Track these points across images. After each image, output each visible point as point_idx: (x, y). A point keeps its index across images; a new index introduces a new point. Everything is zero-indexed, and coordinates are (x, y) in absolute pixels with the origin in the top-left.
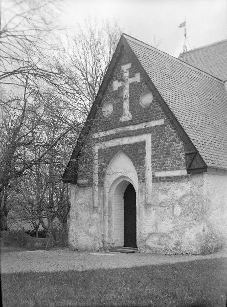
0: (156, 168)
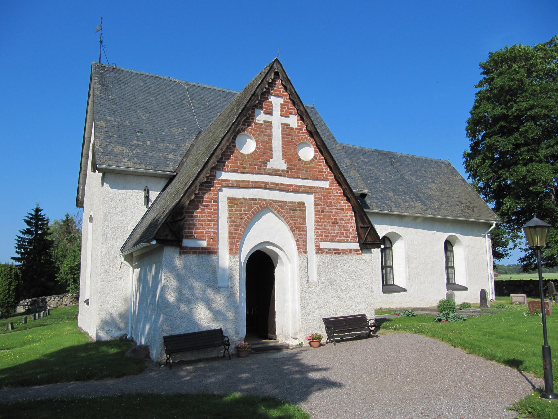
0: (322, 236)
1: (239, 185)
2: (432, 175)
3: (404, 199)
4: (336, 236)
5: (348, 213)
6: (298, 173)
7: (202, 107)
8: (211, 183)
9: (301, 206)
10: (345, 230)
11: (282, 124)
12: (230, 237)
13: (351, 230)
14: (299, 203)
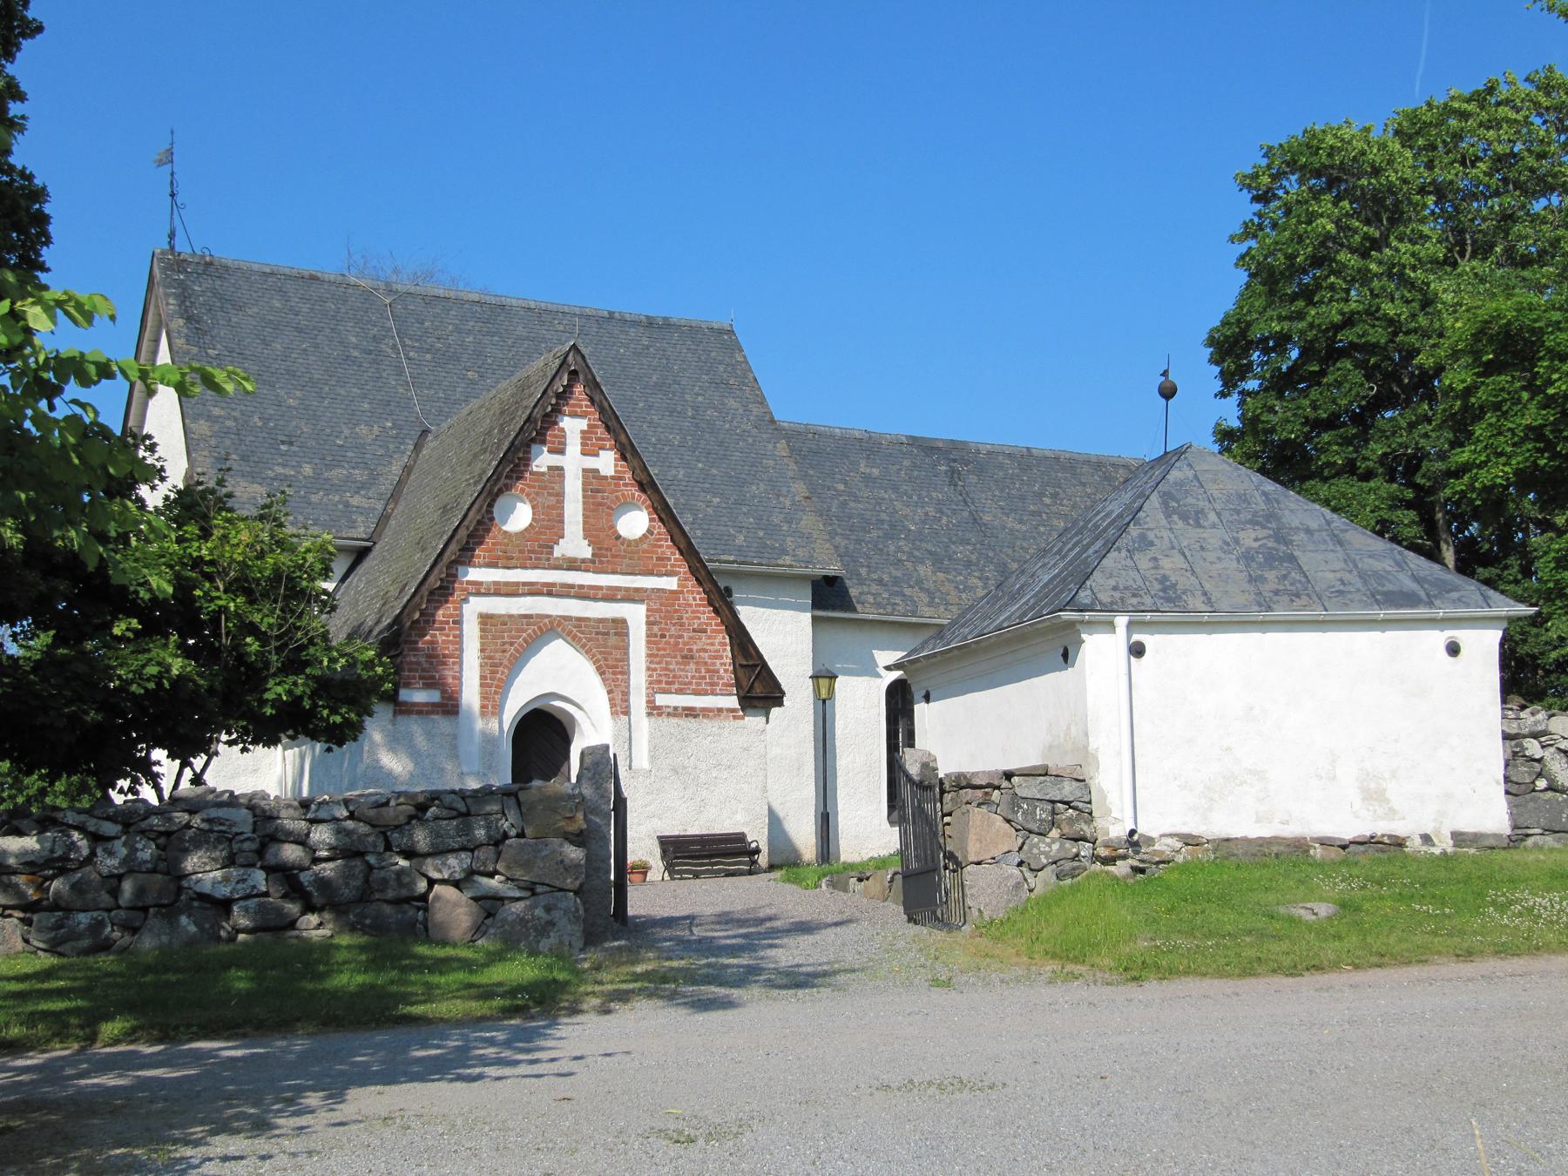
1: (499, 590)
2: (1074, 506)
3: (961, 582)
4: (691, 683)
5: (715, 638)
6: (615, 563)
7: (428, 357)
8: (447, 588)
9: (620, 626)
10: (708, 671)
11: (584, 470)
12: (482, 685)
13: (722, 671)
14: (615, 621)
